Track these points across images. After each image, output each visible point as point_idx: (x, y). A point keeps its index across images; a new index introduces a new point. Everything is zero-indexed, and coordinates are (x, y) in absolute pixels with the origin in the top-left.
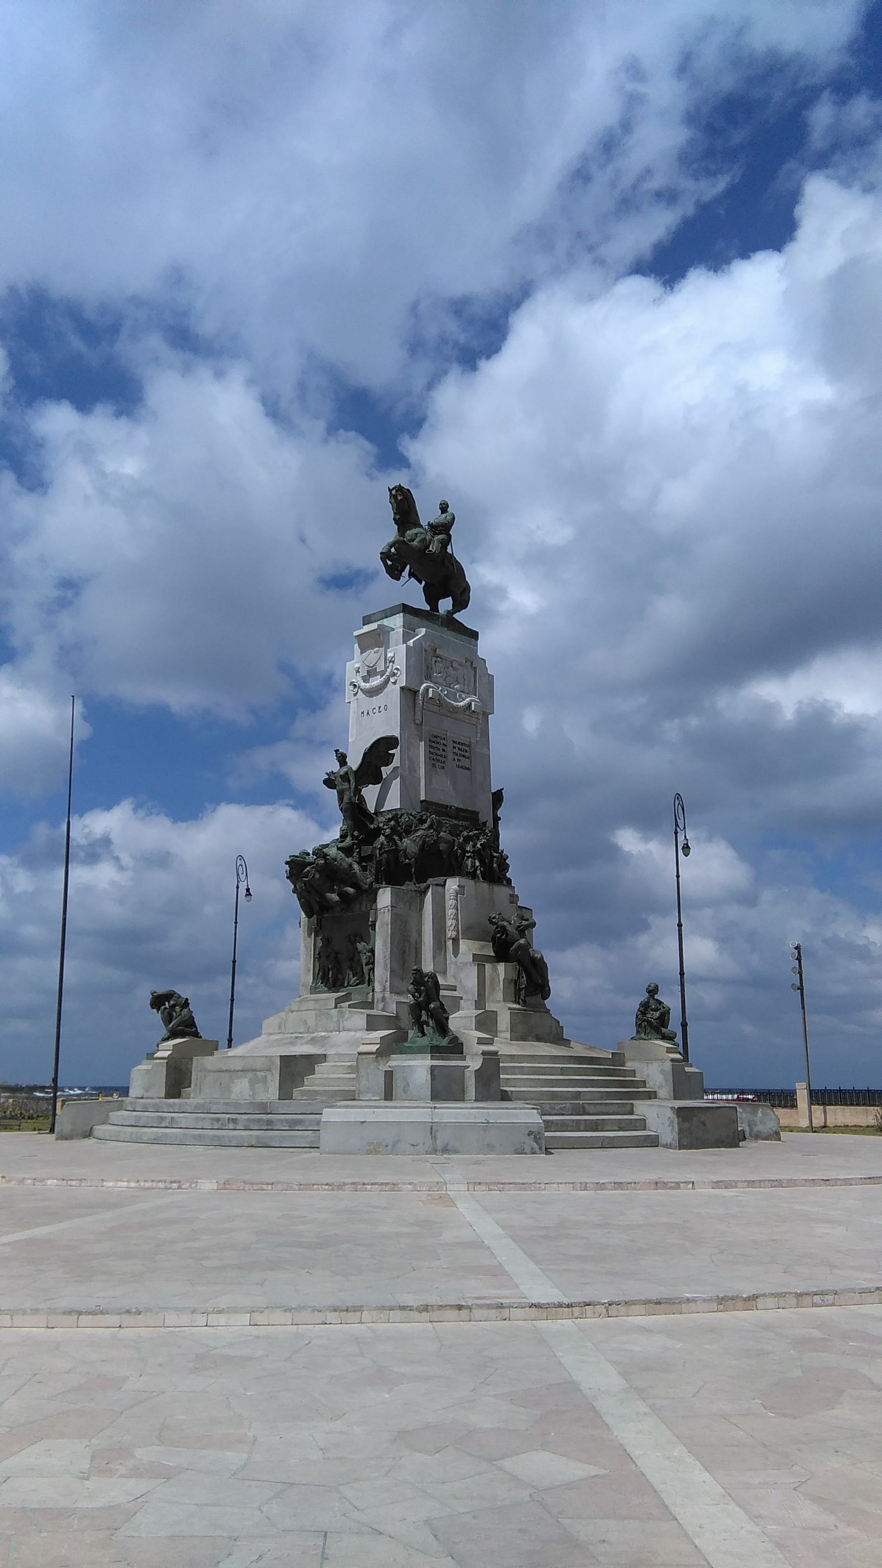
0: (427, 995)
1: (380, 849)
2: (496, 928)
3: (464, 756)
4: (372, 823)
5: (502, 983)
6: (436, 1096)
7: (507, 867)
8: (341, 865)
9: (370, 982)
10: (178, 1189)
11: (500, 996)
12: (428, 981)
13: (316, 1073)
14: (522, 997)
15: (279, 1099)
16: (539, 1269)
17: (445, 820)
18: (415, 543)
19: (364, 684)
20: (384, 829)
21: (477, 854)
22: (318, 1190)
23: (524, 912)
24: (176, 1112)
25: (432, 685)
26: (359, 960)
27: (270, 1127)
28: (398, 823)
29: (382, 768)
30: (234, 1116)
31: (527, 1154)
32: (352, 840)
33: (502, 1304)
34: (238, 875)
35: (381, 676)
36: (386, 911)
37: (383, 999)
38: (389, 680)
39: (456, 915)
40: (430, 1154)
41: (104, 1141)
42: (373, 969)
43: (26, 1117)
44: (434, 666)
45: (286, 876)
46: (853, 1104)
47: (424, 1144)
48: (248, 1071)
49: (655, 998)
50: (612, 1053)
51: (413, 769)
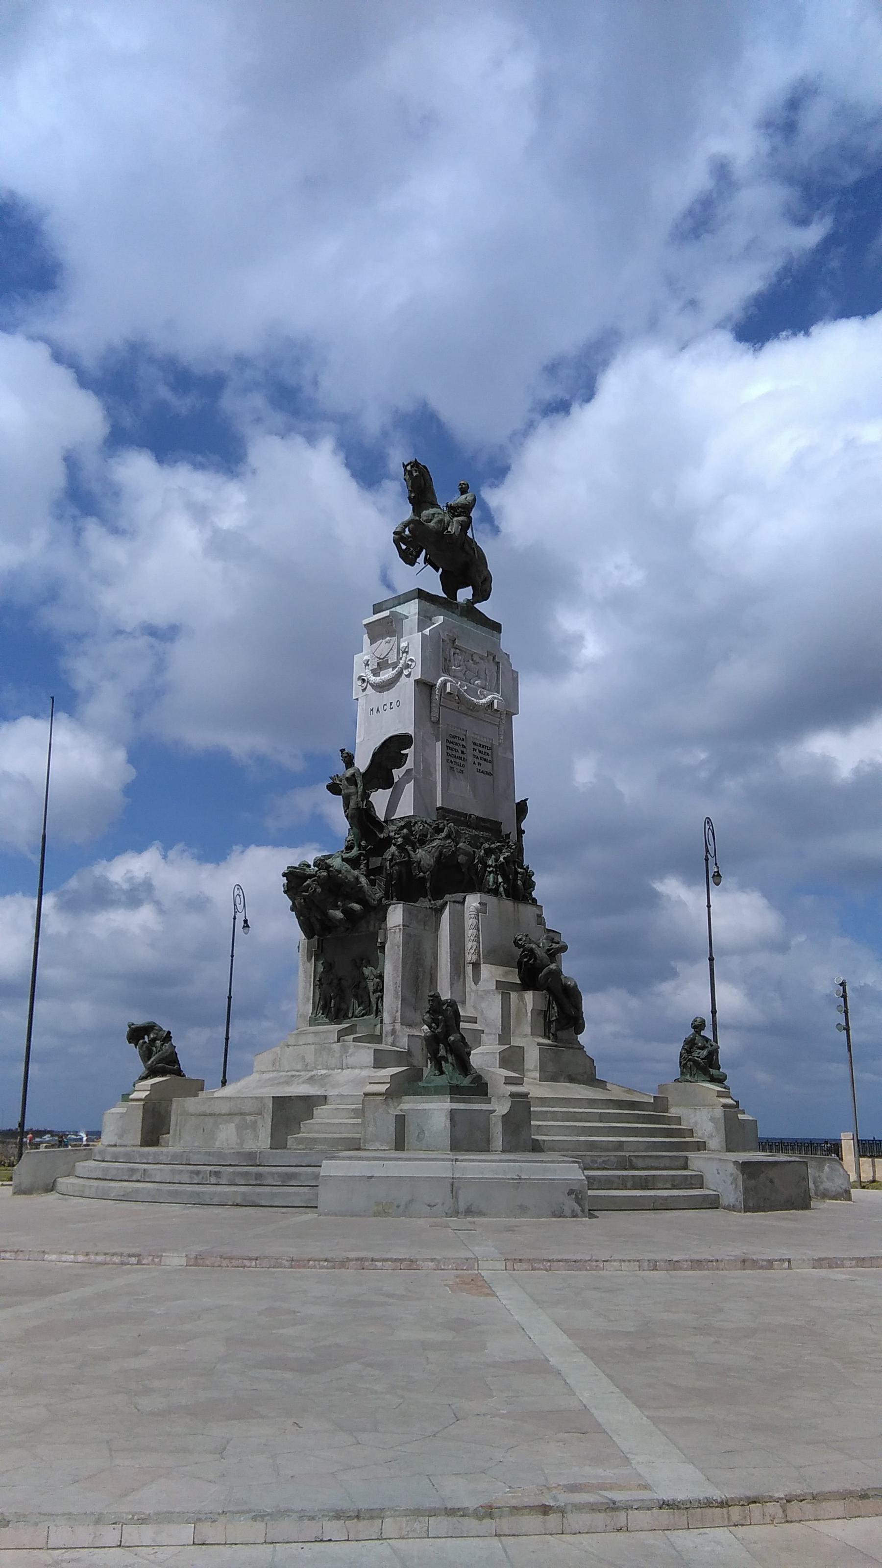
0: (446, 1026)
1: (391, 860)
2: (523, 952)
3: (485, 760)
4: (381, 832)
5: (529, 1014)
6: (456, 1146)
7: (532, 885)
8: (346, 878)
9: (378, 1012)
10: (137, 1264)
11: (528, 1029)
12: (446, 1010)
13: (314, 1117)
14: (553, 1030)
15: (271, 1148)
16: (648, 1417)
17: (463, 829)
18: (432, 524)
19: (374, 678)
20: (395, 838)
21: (500, 869)
22: (314, 1267)
23: (552, 936)
24: (150, 1163)
25: (450, 679)
26: (366, 987)
27: (259, 1182)
28: (411, 832)
29: (393, 771)
30: (217, 1169)
31: (567, 1217)
32: (359, 850)
33: (614, 1503)
34: (235, 905)
35: (394, 669)
36: (397, 930)
37: (393, 1032)
38: (403, 672)
39: (478, 936)
40: (451, 1217)
41: (66, 1196)
42: (382, 997)
43: (6, 1165)
44: (452, 657)
45: (283, 890)
46: (867, 1156)
47: (443, 1204)
48: (236, 1114)
49: (702, 1034)
50: (654, 1097)
51: (428, 771)
